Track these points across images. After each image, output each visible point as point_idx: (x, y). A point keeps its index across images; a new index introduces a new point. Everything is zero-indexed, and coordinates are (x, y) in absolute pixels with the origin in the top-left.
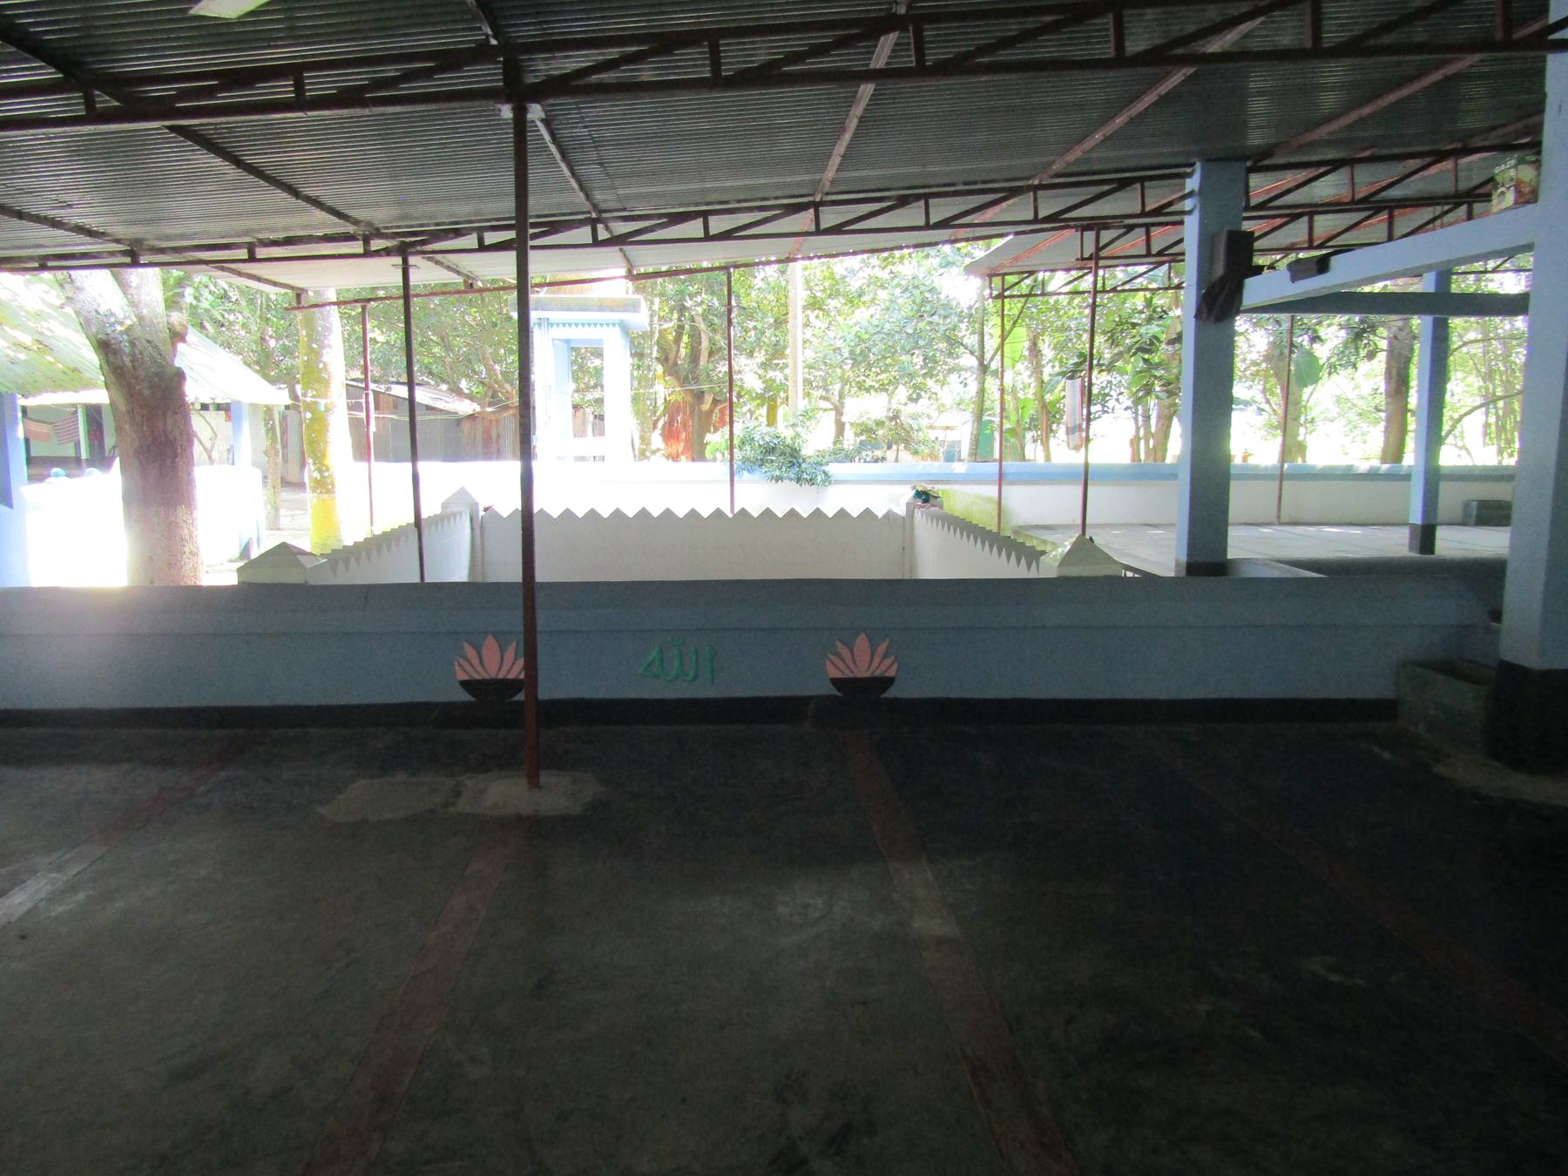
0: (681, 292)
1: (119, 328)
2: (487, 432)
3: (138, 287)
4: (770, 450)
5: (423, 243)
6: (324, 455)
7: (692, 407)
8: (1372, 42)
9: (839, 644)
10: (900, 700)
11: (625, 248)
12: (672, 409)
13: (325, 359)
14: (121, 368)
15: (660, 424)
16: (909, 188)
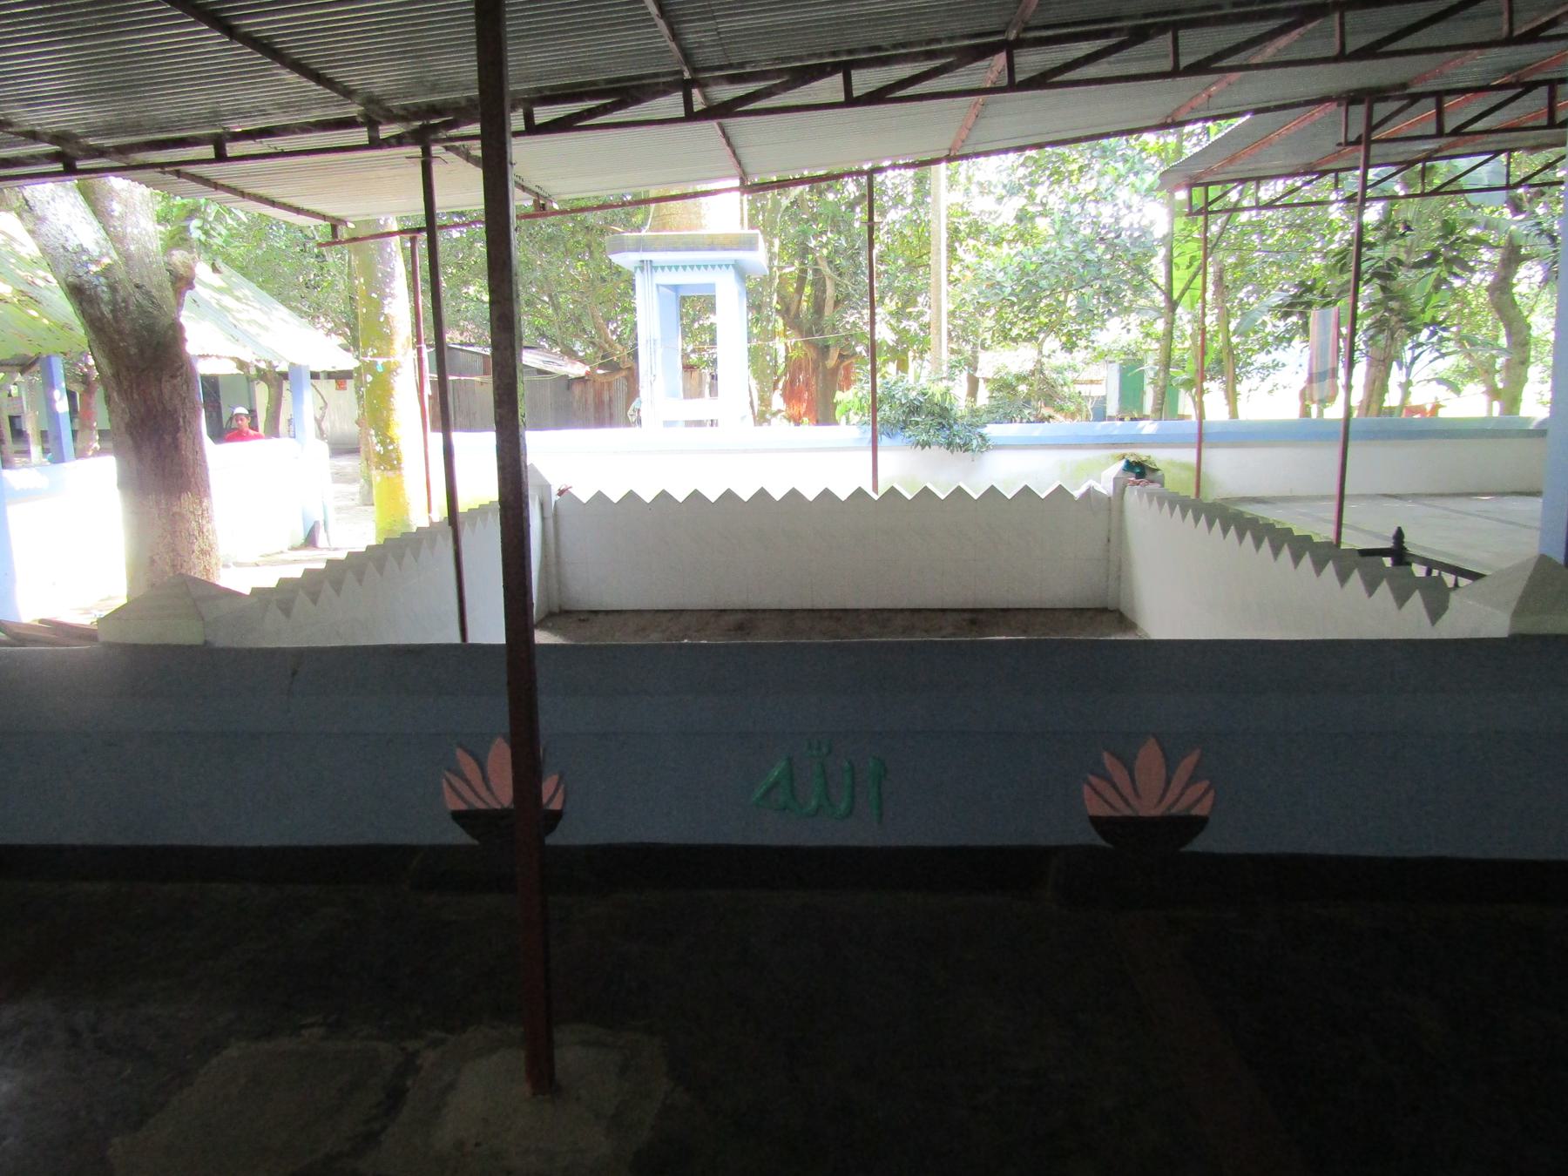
0: (804, 233)
1: (94, 268)
2: (598, 395)
3: (122, 217)
4: (914, 409)
5: (449, 125)
6: (387, 425)
7: (815, 362)
8: (1385, 49)
9: (1107, 758)
10: (1213, 856)
11: (725, 121)
12: (794, 367)
13: (386, 311)
14: (100, 320)
15: (781, 385)
16: (1146, 16)
